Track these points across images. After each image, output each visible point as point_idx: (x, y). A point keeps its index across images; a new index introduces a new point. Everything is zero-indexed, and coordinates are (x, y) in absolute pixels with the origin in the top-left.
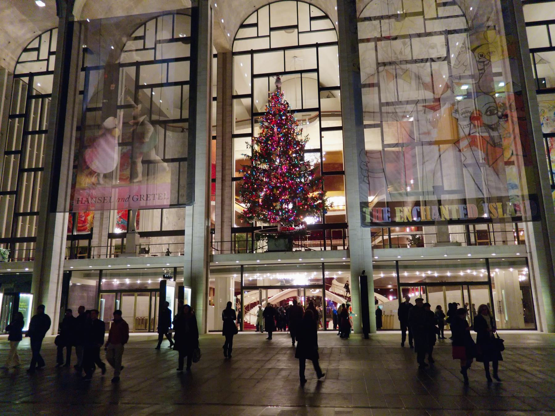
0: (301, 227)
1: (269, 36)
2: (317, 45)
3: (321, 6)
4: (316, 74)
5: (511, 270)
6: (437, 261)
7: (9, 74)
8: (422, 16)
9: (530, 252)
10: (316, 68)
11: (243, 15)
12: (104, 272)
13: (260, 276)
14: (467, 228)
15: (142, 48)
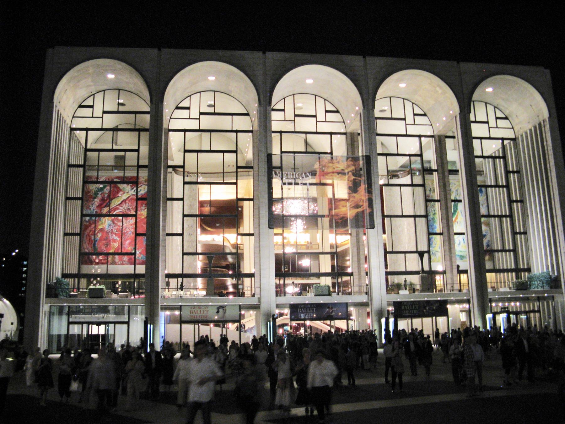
0: (39, 372)
1: (102, 117)
2: (185, 131)
7: (69, 127)
9: (472, 297)
14: (480, 381)
15: (407, 123)
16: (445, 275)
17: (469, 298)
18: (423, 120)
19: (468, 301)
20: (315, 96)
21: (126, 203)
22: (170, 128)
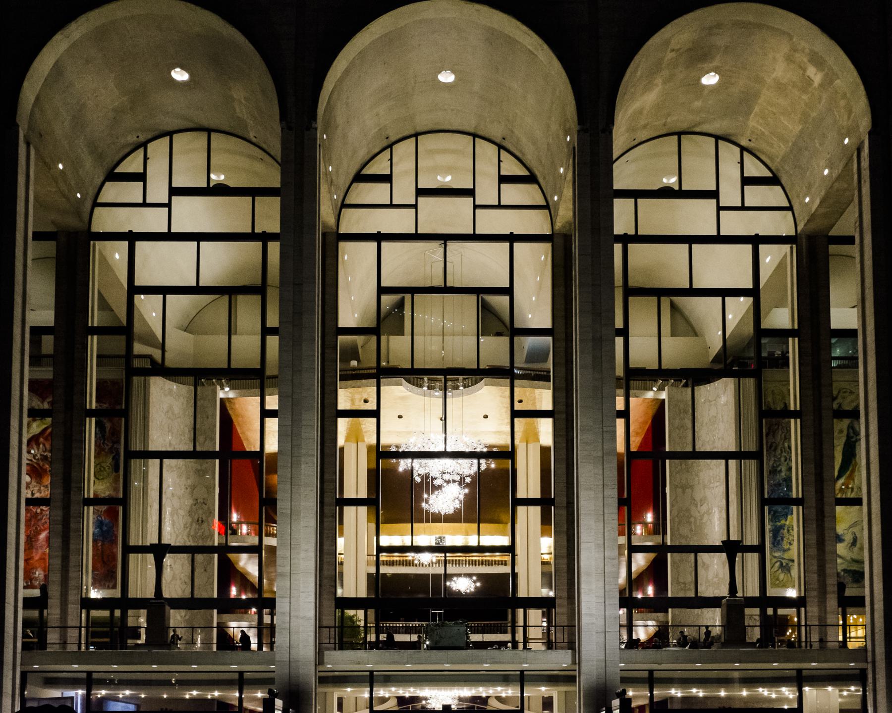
1: (168, 205)
3: (523, 154)
4: (506, 298)
5: (830, 689)
6: (751, 671)
8: (715, 201)
9: (874, 662)
10: (506, 284)
11: (362, 154)
12: (805, 673)
13: (502, 690)
16: (803, 610)
17: (862, 665)
18: (773, 195)
19: (860, 678)
20: (475, 136)
21: (38, 444)
22: (342, 231)
